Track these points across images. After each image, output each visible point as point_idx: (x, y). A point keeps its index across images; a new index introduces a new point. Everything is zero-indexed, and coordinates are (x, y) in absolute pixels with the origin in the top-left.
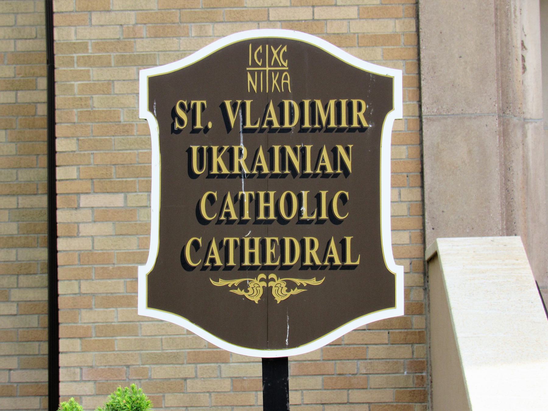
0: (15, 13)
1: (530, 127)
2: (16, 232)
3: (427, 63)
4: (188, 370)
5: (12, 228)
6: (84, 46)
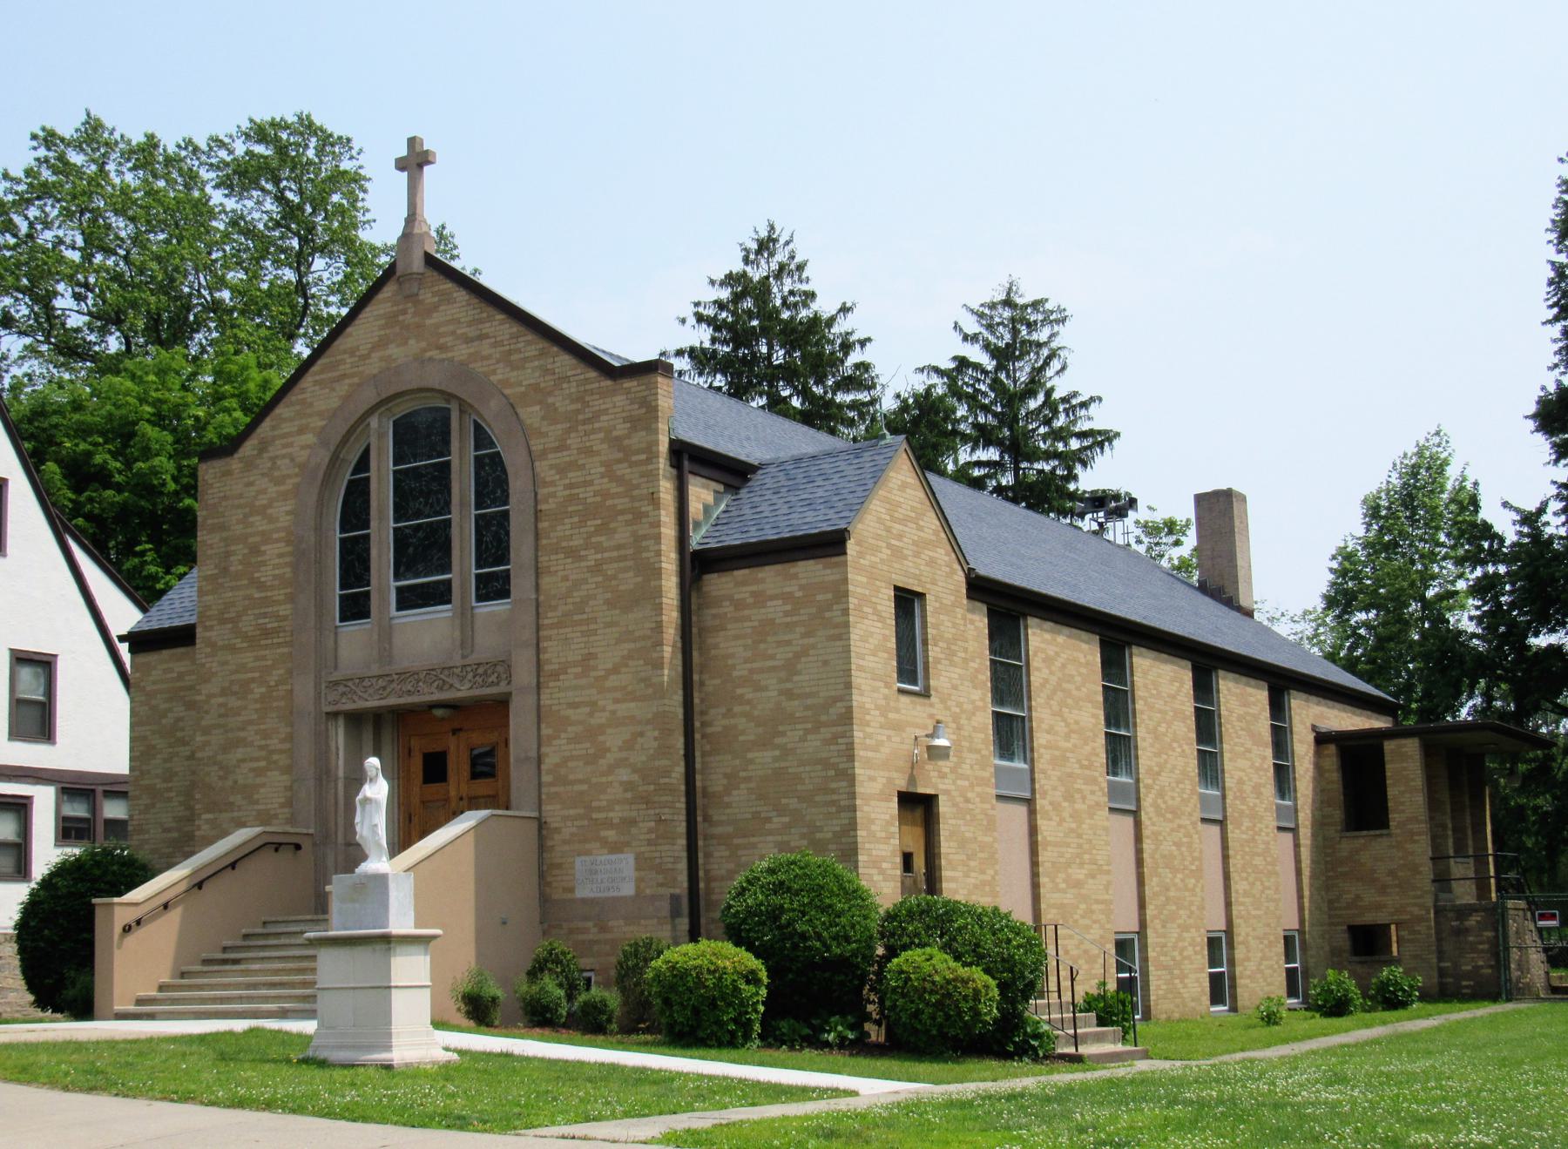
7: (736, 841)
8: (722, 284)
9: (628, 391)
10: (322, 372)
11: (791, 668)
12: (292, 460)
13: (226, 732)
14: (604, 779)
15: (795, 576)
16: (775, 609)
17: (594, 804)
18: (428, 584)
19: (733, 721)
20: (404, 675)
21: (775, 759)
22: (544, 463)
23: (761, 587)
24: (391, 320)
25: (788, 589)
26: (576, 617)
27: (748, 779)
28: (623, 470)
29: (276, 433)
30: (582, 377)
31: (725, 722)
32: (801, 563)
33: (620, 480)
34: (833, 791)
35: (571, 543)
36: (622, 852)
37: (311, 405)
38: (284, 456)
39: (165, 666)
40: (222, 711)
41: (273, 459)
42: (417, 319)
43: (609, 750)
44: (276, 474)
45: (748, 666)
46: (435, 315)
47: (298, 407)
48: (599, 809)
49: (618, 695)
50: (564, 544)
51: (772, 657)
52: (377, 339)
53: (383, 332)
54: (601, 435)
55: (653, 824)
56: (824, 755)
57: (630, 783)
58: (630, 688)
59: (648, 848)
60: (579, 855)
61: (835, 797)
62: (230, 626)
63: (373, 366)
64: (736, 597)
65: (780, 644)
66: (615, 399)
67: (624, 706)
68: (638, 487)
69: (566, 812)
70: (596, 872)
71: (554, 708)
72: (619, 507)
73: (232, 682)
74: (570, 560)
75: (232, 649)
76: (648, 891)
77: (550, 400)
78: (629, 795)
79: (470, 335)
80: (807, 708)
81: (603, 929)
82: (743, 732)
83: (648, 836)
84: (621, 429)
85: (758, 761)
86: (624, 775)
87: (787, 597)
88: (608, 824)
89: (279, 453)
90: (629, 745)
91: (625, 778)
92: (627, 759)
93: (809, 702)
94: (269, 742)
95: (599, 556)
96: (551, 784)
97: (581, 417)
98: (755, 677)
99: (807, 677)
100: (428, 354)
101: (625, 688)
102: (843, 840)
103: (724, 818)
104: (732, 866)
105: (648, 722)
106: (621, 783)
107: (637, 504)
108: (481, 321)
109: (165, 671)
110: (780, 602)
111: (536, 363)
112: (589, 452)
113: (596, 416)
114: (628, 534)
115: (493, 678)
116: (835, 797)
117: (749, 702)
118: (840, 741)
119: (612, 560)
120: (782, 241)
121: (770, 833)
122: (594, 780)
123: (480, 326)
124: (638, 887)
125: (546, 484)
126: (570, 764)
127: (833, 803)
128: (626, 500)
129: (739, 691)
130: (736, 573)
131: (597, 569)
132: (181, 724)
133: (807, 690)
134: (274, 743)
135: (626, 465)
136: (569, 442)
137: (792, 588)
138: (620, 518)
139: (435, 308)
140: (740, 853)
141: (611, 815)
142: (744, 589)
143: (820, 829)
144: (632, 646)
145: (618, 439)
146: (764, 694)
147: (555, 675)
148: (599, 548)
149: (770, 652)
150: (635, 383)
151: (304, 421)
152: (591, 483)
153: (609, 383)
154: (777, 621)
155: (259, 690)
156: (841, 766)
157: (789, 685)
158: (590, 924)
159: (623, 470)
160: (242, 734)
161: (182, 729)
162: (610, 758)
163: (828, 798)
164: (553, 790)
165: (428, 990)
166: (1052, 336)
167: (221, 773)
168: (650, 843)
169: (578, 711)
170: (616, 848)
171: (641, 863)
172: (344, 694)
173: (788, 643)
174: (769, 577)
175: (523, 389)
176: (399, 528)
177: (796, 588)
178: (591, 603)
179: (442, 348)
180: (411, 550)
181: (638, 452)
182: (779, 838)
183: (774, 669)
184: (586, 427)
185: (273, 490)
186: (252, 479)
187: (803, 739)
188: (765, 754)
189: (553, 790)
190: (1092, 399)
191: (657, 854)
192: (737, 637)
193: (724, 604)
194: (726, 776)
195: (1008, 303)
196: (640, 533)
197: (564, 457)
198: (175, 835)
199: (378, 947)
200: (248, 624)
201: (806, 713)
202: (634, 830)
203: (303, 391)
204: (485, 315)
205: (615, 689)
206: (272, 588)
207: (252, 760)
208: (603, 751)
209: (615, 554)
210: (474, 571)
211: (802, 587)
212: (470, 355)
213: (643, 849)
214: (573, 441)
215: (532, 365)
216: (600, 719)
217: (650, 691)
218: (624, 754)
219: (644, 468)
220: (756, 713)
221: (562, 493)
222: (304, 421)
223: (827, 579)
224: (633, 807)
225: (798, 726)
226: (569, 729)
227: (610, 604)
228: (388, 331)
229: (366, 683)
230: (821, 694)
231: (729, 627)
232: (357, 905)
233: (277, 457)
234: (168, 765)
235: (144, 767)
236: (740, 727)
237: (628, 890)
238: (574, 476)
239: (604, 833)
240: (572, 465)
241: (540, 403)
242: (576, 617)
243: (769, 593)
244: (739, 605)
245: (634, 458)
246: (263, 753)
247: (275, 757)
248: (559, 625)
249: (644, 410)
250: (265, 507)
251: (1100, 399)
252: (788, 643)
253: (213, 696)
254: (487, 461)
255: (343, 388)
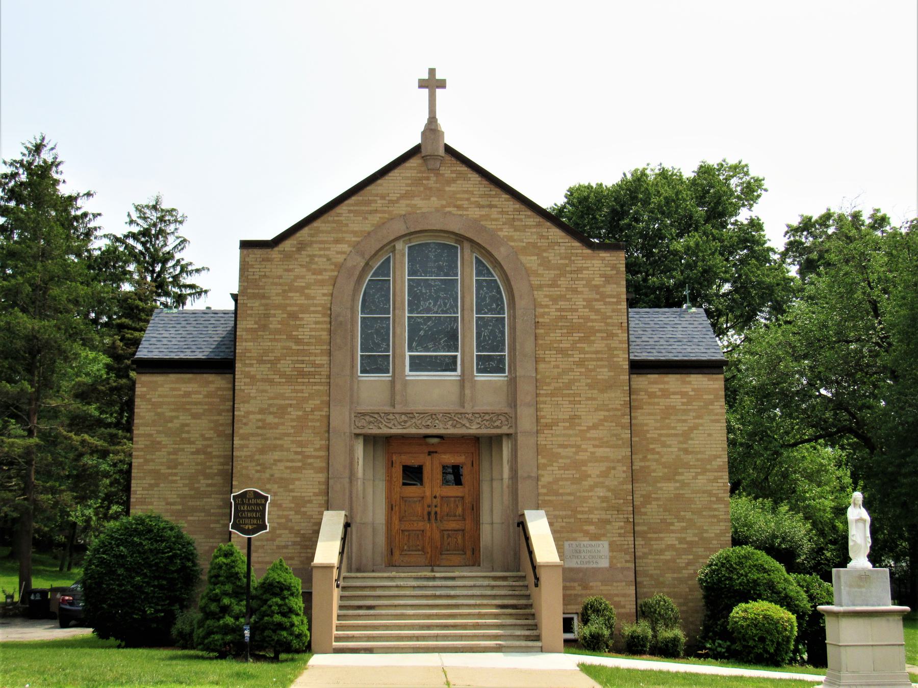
0: (235, 331)
1: (359, 481)
2: (619, 259)
3: (842, 273)
4: (265, 543)
5: (221, 503)
6: (241, 457)
7: (649, 535)
8: (11, 164)
9: (603, 259)
10: (356, 204)
11: (686, 436)
12: (329, 259)
13: (266, 439)
14: (586, 494)
15: (689, 383)
16: (676, 400)
17: (579, 509)
18: (436, 356)
19: (647, 464)
20: (410, 415)
21: (677, 488)
22: (540, 293)
23: (667, 386)
24: (417, 182)
25: (685, 390)
26: (565, 392)
27: (657, 499)
28: (599, 305)
29: (314, 239)
30: (570, 244)
31: (643, 464)
32: (692, 376)
33: (597, 312)
34: (715, 510)
35: (561, 345)
36: (599, 540)
37: (347, 225)
38: (320, 256)
39: (173, 386)
40: (260, 424)
41: (312, 257)
42: (438, 185)
43: (590, 476)
44: (314, 266)
45: (659, 432)
46: (452, 185)
47: (335, 225)
48: (583, 512)
49: (597, 443)
50: (555, 345)
51: (674, 428)
52: (404, 192)
53: (409, 188)
54: (585, 282)
55: (622, 524)
56: (709, 488)
57: (606, 497)
58: (605, 439)
59: (619, 538)
60: (567, 540)
61: (716, 513)
62: (269, 365)
63: (402, 208)
64: (650, 390)
65: (679, 421)
66: (593, 262)
67: (601, 450)
68: (611, 317)
69: (557, 513)
70: (580, 552)
71: (548, 447)
72: (597, 328)
73: (270, 405)
74: (560, 356)
75: (271, 382)
76: (619, 565)
77: (545, 254)
78: (604, 505)
79: (481, 203)
80: (698, 460)
81: (586, 587)
82: (654, 471)
83: (619, 531)
84: (598, 281)
85: (664, 488)
86: (601, 492)
87: (683, 394)
88: (589, 522)
89: (317, 253)
90: (605, 474)
91: (601, 494)
92: (603, 483)
93: (699, 456)
94: (304, 450)
95: (582, 356)
96: (545, 494)
97: (568, 269)
98: (663, 439)
99: (698, 442)
100: (447, 209)
101: (601, 439)
102: (722, 539)
103: (641, 521)
104: (646, 550)
105: (618, 461)
106: (599, 497)
107: (610, 328)
108: (490, 196)
109: (173, 389)
110: (679, 397)
111: (535, 230)
112: (575, 291)
113: (579, 270)
114: (604, 345)
115: (498, 423)
116: (716, 513)
117: (658, 453)
118: (719, 481)
119: (592, 360)
120: (49, 147)
121: (673, 532)
122: (578, 494)
123: (490, 199)
124: (611, 562)
125: (542, 306)
126: (561, 483)
127: (714, 516)
128: (603, 324)
129: (651, 446)
130: (649, 376)
131: (581, 363)
132: (186, 428)
133: (698, 450)
134: (309, 450)
135: (602, 303)
136: (559, 282)
137: (688, 389)
138: (598, 335)
139: (454, 181)
140: (652, 543)
141: (591, 516)
142: (655, 386)
143: (707, 531)
144: (607, 413)
145: (596, 286)
146: (669, 449)
147: (549, 426)
148: (582, 351)
149: (672, 425)
150: (608, 255)
151: (340, 235)
152: (576, 310)
153: (589, 251)
154: (677, 407)
155: (295, 413)
156: (720, 495)
157: (685, 446)
158: (576, 584)
159: (599, 305)
160: (278, 442)
161: (188, 432)
162: (590, 481)
163: (712, 513)
164: (547, 498)
165: (902, 649)
166: (176, 229)
167: (259, 468)
168: (620, 535)
169: (567, 450)
170: (595, 537)
171: (613, 547)
172: (370, 422)
173: (685, 421)
174: (672, 381)
175: (524, 244)
176: (412, 317)
177: (690, 390)
178: (576, 384)
179: (459, 207)
180: (422, 333)
181: (611, 296)
182: (679, 535)
183: (676, 435)
184: (572, 275)
185: (311, 278)
186: (291, 267)
187: (695, 478)
188: (669, 485)
189: (547, 498)
190: (203, 269)
191: (626, 543)
192: (650, 414)
193: (641, 393)
194: (642, 496)
195: (155, 208)
196: (612, 345)
197: (555, 292)
198: (180, 507)
199: (891, 618)
200: (286, 366)
201: (696, 463)
202: (608, 527)
203: (339, 215)
204: (494, 193)
205: (595, 439)
206: (308, 344)
207: (288, 461)
208: (586, 476)
209: (594, 356)
210: (459, 354)
211: (693, 390)
212: (481, 216)
213: (614, 539)
214: (562, 282)
215: (531, 230)
216: (583, 456)
217: (620, 442)
218: (601, 480)
219: (615, 307)
220: (663, 460)
221: (554, 314)
222: (340, 235)
223: (710, 386)
224: (608, 512)
225: (691, 470)
226: (560, 461)
227: (591, 386)
228: (413, 188)
229: (391, 417)
230: (707, 453)
231: (644, 407)
232: (864, 590)
233: (315, 256)
234: (172, 457)
235: (148, 457)
236: (652, 467)
237: (604, 563)
238: (562, 304)
239: (586, 528)
240: (562, 297)
241: (537, 255)
242: (565, 392)
243: (671, 390)
244: (652, 395)
245: (608, 300)
246: (300, 457)
247: (310, 461)
248: (552, 395)
249: (614, 272)
250: (304, 288)
251: (208, 269)
252: (685, 421)
253: (253, 413)
254: (485, 284)
255: (375, 219)
